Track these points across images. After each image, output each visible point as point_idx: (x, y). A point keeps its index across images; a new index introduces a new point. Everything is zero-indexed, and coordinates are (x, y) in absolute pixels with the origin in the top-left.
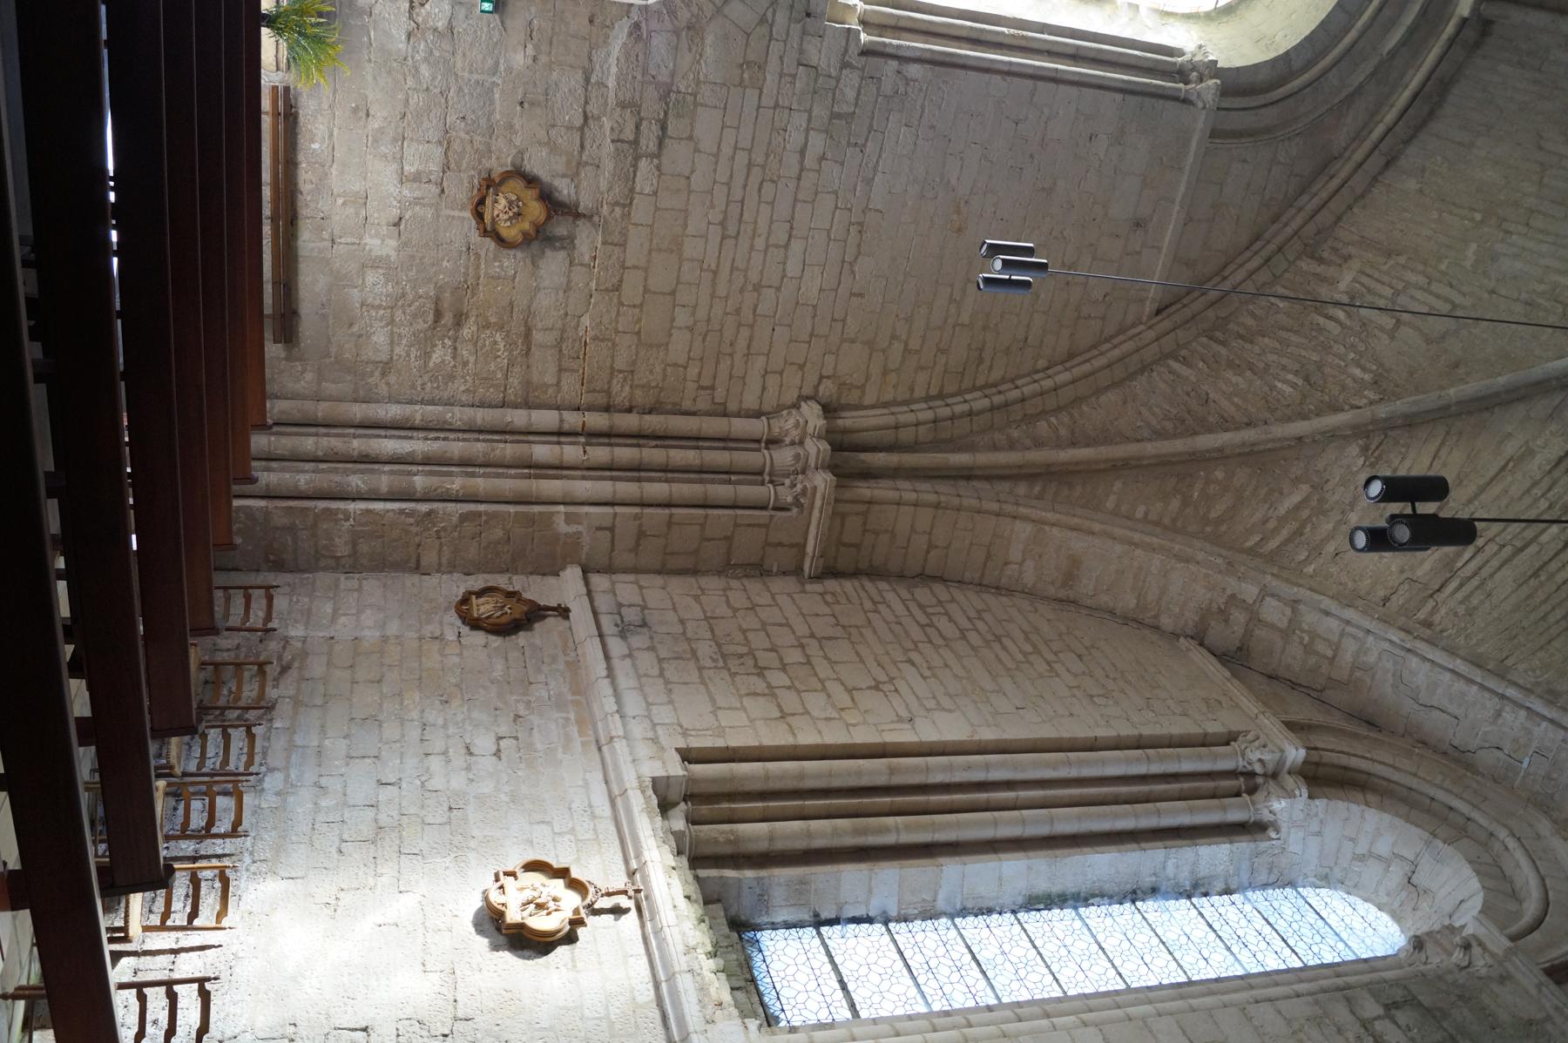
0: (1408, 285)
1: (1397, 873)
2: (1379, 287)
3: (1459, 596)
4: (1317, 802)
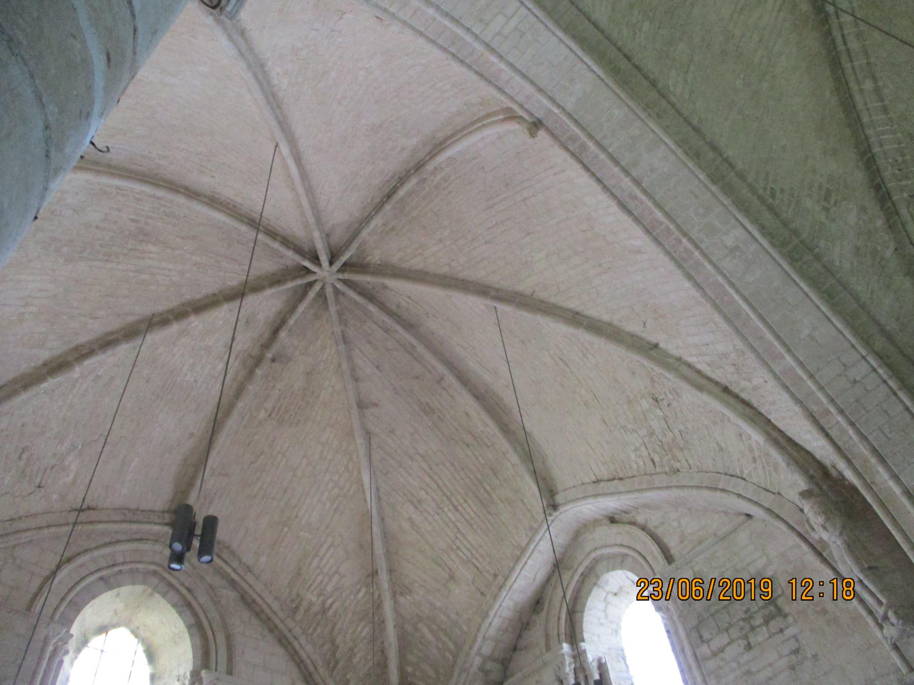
1: (611, 598)
2: (318, 581)
3: (481, 559)
4: (585, 637)
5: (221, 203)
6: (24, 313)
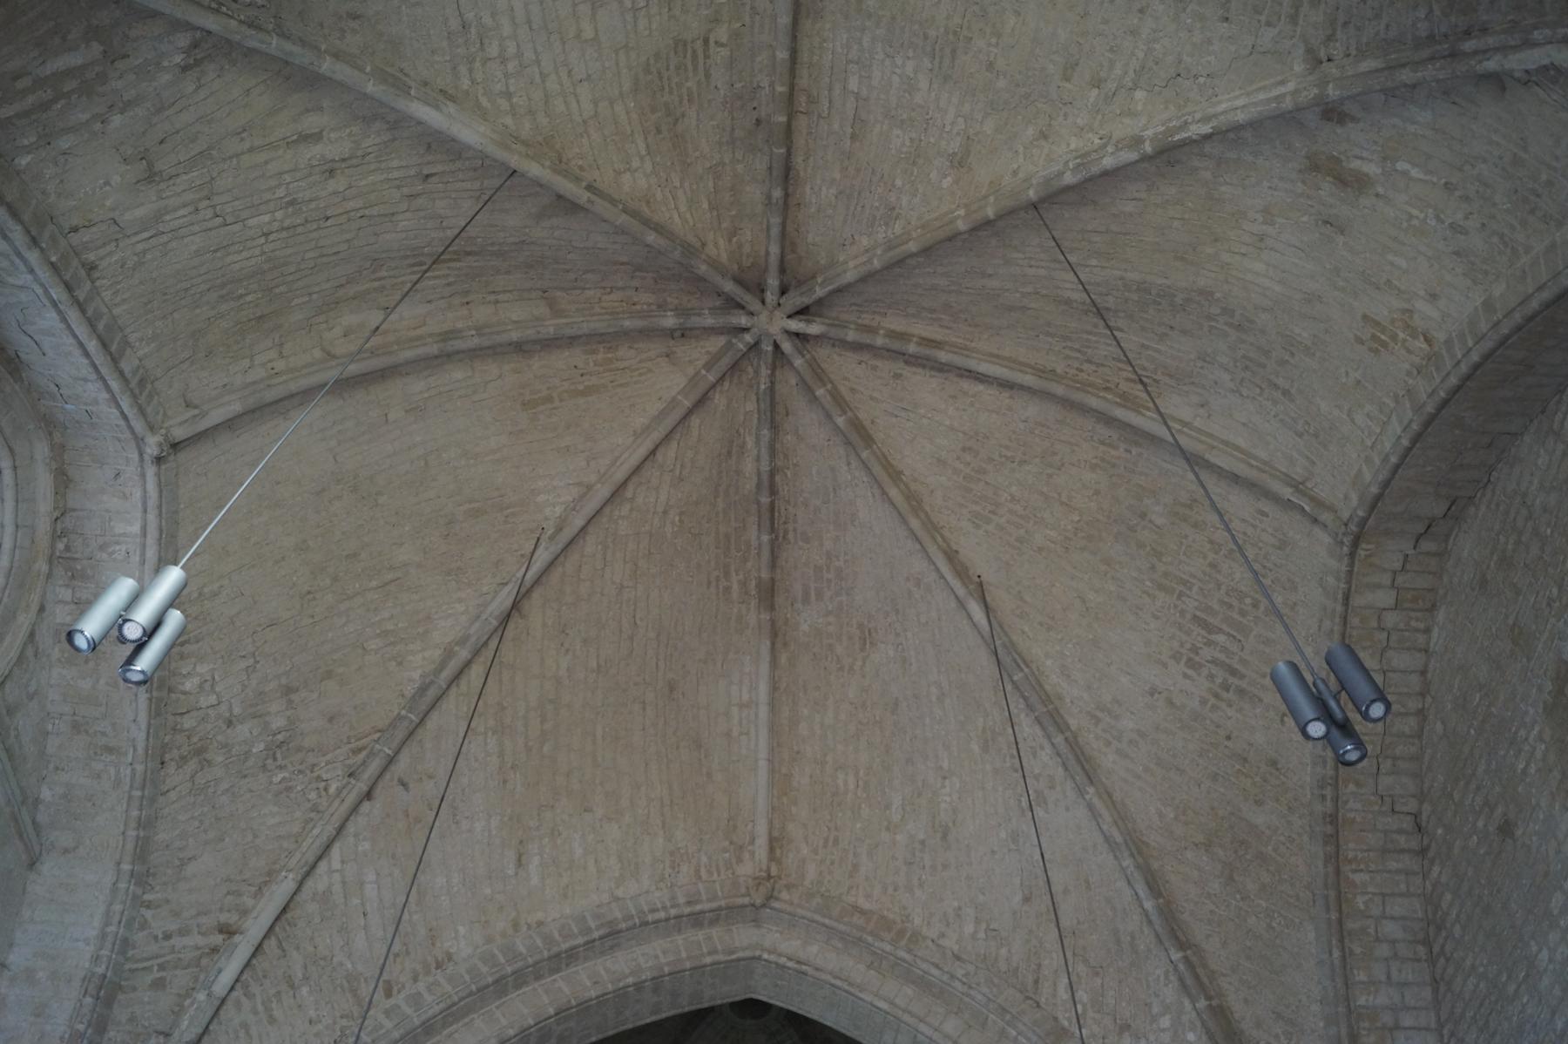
6: (1265, 223)
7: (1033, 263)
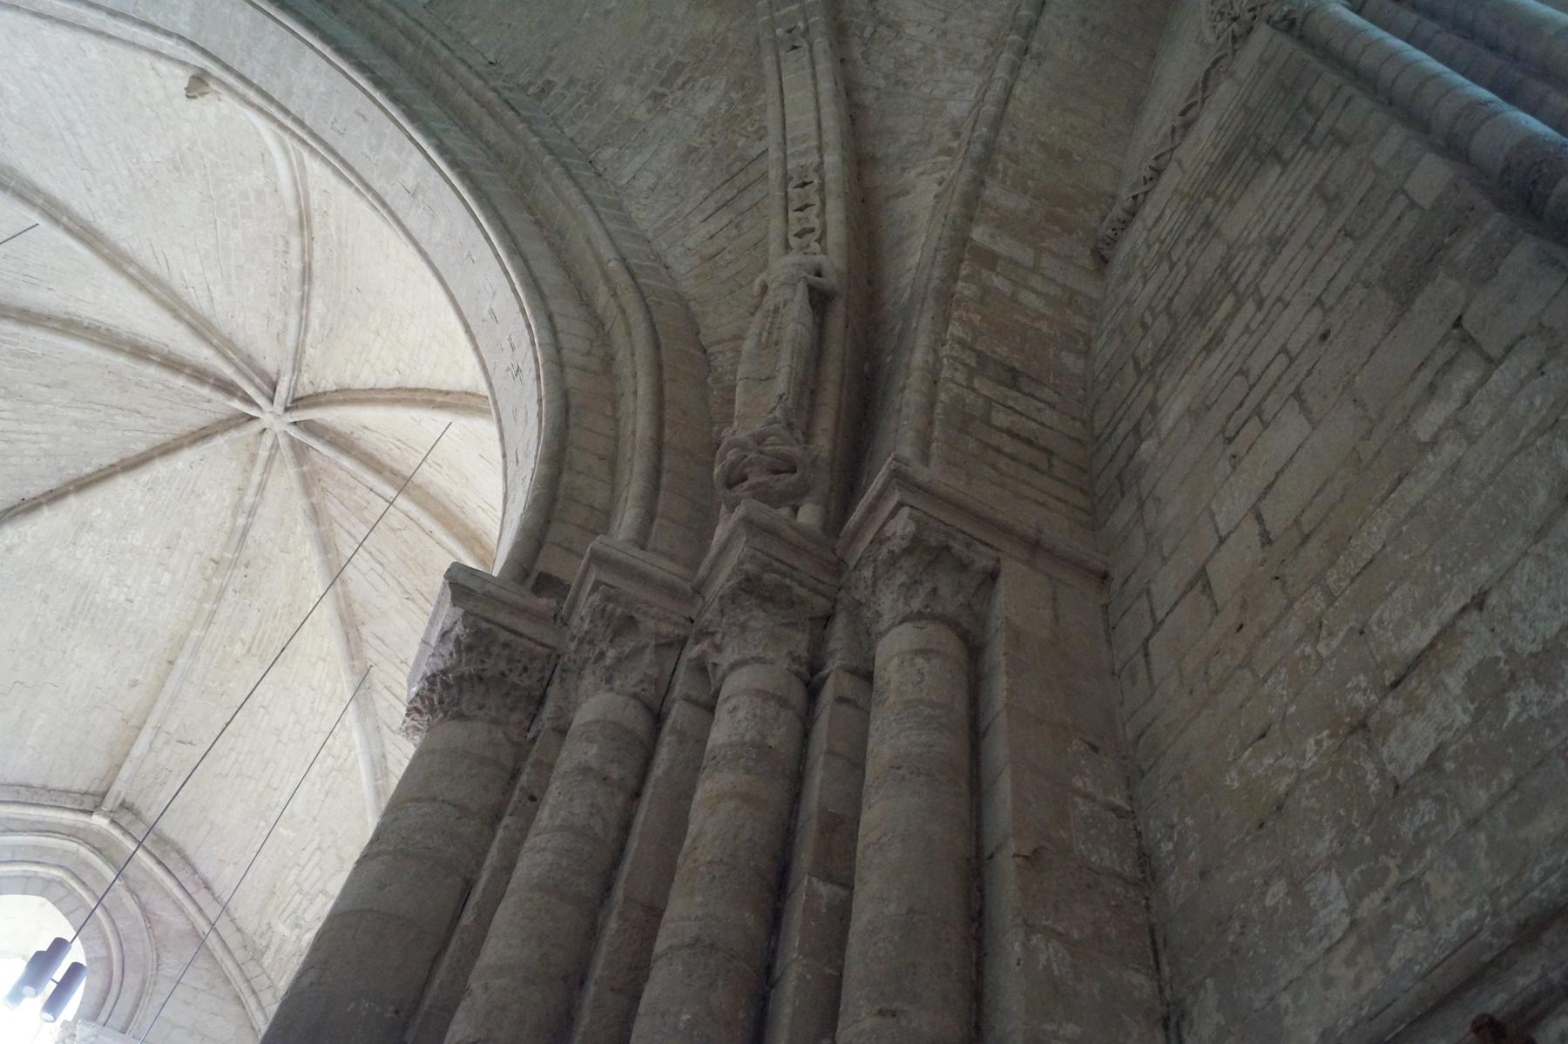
0: (296, 882)
2: (294, 905)
5: (87, 328)
7: (33, 438)
